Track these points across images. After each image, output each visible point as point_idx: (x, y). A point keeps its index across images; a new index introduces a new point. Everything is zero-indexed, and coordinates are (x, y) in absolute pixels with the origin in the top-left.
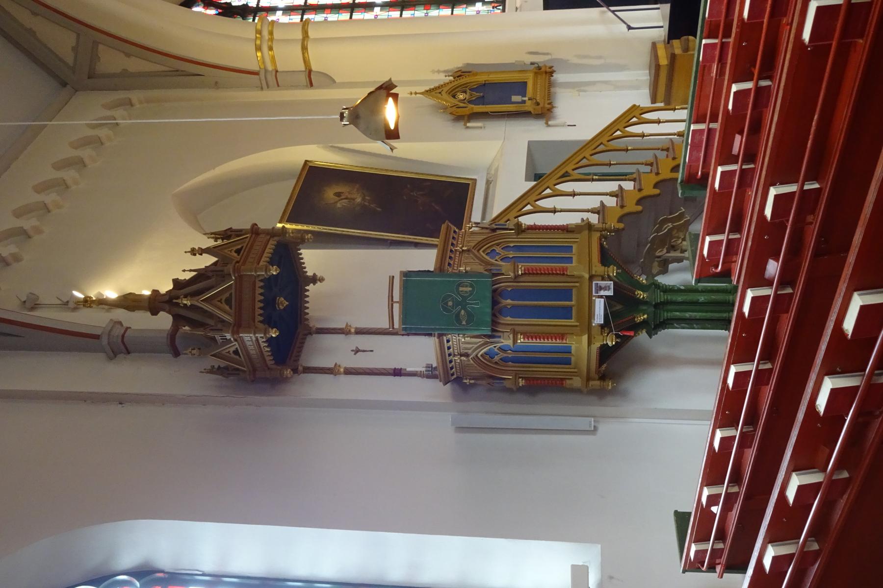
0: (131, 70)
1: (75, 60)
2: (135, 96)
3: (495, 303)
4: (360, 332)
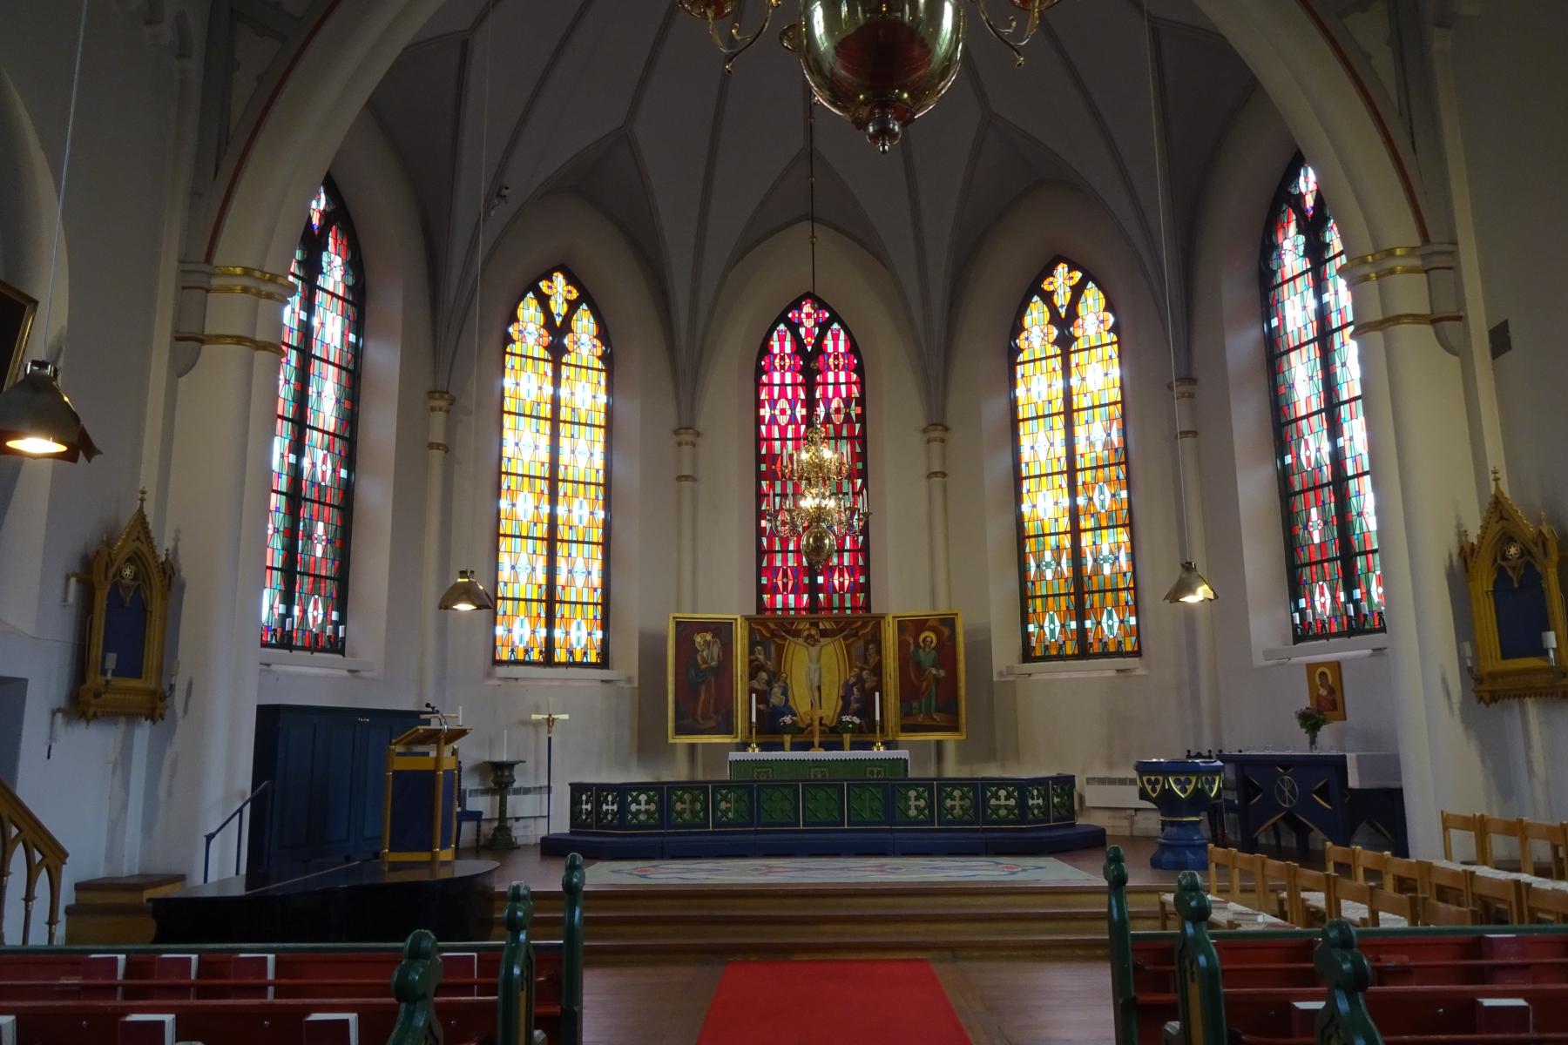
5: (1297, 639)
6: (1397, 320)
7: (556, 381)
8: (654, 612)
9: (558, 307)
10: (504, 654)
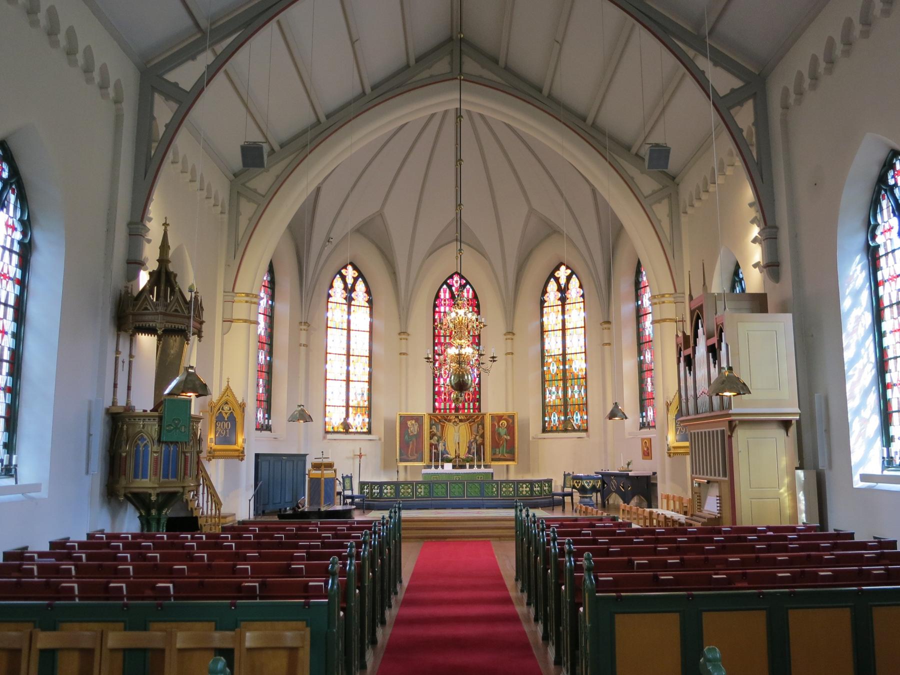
0: (241, 217)
1: (248, 188)
2: (226, 217)
3: (172, 443)
4: (130, 363)
5: (641, 428)
6: (664, 320)
7: (349, 313)
8: (389, 409)
9: (350, 281)
10: (329, 428)
